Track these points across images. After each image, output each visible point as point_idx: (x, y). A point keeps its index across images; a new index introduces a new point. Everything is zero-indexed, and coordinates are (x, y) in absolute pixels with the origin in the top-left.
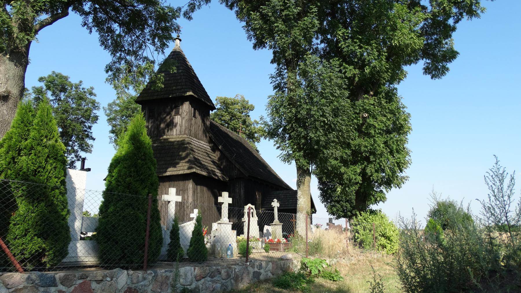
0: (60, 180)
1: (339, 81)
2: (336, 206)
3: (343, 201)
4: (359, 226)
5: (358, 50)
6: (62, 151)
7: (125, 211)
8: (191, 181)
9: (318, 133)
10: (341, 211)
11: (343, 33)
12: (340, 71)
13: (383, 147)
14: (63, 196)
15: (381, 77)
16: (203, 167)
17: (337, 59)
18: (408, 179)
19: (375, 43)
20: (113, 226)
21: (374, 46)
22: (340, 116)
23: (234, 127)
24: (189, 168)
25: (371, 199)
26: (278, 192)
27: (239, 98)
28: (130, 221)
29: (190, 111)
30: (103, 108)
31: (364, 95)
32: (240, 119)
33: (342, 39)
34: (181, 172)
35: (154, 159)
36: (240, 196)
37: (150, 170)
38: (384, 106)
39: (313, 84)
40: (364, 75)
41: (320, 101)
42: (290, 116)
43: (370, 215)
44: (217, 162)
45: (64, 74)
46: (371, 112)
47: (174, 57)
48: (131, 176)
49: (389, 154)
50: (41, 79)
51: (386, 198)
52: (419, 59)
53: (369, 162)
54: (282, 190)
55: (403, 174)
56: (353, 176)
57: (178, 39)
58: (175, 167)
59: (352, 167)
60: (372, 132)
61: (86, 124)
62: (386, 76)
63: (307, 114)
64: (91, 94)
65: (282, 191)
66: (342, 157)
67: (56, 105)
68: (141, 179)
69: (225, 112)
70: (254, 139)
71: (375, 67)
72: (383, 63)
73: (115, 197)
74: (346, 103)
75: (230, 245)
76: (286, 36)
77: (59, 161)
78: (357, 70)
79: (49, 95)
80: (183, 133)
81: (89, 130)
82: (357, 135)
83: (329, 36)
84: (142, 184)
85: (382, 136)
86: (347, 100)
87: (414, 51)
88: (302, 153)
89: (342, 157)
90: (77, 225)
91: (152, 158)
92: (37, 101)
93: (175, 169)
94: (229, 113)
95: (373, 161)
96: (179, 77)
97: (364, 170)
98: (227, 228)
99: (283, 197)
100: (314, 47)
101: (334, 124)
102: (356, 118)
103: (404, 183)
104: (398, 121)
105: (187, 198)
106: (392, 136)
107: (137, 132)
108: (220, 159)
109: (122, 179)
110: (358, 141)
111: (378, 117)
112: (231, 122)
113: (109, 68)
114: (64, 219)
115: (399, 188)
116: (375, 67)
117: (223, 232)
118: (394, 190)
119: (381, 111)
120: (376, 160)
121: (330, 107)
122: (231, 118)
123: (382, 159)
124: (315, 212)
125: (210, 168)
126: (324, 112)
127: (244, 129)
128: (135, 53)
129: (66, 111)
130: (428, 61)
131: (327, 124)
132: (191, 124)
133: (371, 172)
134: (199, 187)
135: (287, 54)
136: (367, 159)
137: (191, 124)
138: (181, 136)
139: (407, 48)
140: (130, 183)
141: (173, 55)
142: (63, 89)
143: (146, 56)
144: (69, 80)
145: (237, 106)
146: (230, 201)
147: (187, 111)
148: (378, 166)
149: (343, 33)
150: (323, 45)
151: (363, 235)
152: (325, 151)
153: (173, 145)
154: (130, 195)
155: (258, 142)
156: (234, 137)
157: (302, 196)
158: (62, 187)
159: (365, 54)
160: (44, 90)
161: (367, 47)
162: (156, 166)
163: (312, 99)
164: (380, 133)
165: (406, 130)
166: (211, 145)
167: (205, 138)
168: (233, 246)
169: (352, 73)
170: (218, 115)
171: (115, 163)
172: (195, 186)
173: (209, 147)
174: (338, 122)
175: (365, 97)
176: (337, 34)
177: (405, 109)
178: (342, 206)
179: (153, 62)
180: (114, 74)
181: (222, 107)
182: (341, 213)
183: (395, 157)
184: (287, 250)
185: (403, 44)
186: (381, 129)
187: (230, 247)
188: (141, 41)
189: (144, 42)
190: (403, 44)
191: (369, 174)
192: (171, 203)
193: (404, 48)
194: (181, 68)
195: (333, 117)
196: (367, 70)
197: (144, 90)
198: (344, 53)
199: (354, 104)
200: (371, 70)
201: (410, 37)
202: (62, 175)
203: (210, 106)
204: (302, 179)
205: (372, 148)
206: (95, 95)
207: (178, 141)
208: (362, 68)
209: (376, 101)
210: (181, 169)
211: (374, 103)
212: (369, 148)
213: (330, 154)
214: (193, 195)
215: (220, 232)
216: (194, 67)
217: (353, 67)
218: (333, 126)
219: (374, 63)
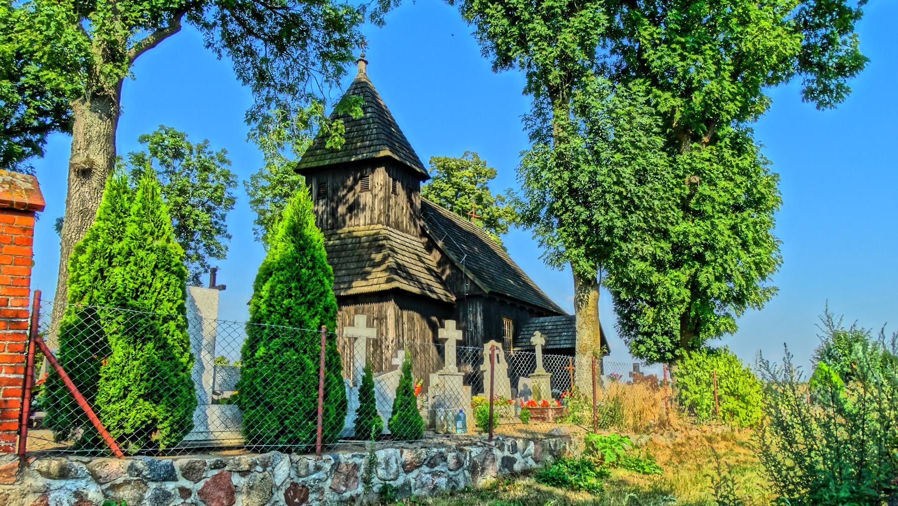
0: (176, 306)
1: (646, 120)
3: (657, 334)
6: (178, 257)
8: (392, 302)
10: (655, 352)
14: (181, 332)
16: (410, 277)
24: (389, 280)
26: (542, 319)
29: (386, 184)
32: (473, 193)
33: (649, 46)
36: (475, 327)
37: (323, 284)
44: (435, 269)
48: (290, 296)
49: (740, 247)
53: (704, 263)
54: (547, 316)
55: (767, 284)
59: (674, 273)
60: (708, 208)
61: (216, 212)
63: (590, 181)
73: (266, 331)
74: (659, 160)
78: (678, 99)
81: (221, 222)
85: (727, 216)
86: (661, 153)
87: (784, 59)
89: (654, 256)
93: (364, 283)
94: (453, 184)
95: (712, 261)
96: (366, 126)
97: (694, 277)
98: (455, 382)
101: (638, 197)
102: (678, 185)
105: (387, 333)
110: (683, 226)
113: (252, 117)
115: (759, 309)
117: (449, 389)
118: (750, 311)
122: (457, 193)
125: (423, 281)
126: (619, 176)
128: (291, 89)
131: (626, 198)
132: (389, 206)
134: (405, 313)
136: (699, 257)
138: (372, 226)
140: (290, 308)
142: (178, 154)
148: (720, 269)
149: (651, 35)
153: (360, 242)
154: (290, 328)
158: (180, 317)
159: (693, 70)
161: (694, 57)
162: (333, 278)
164: (723, 211)
174: (645, 192)
178: (656, 343)
182: (655, 355)
186: (724, 204)
187: (461, 414)
199: (674, 161)
200: (704, 97)
201: (775, 33)
208: (687, 94)
217: (670, 94)
219: (711, 85)
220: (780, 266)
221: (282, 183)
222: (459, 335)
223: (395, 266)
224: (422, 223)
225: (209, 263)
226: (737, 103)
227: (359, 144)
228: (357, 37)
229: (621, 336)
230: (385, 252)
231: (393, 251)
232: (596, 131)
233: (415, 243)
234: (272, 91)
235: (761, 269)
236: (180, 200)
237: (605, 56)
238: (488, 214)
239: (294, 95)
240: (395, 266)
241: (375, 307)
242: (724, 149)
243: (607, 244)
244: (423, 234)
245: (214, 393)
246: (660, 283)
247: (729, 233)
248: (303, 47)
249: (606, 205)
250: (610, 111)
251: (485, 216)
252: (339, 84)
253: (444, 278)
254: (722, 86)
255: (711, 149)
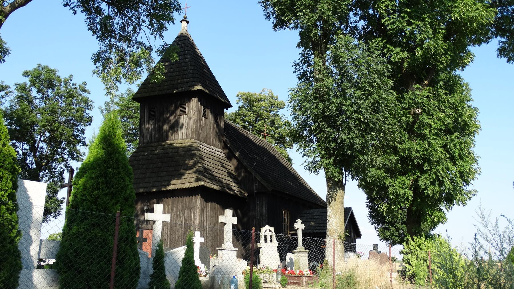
0: (7, 194)
1: (380, 68)
2: (390, 229)
3: (398, 223)
4: (410, 255)
5: (407, 27)
6: (11, 158)
7: (90, 232)
8: (199, 196)
9: (352, 134)
10: (397, 236)
11: (387, 6)
12: (383, 55)
13: (441, 152)
14: (11, 214)
15: (438, 62)
16: (213, 178)
17: (380, 39)
18: (476, 193)
19: (429, 17)
20: (75, 251)
21: (428, 21)
22: (381, 112)
23: (260, 129)
24: (197, 180)
25: (427, 220)
26: (311, 211)
27: (266, 94)
28: (96, 246)
29: (199, 110)
30: (100, 108)
31: (415, 84)
32: (268, 119)
33: (385, 14)
34: (187, 186)
35: (130, 167)
36: (262, 215)
37: (124, 181)
38: (442, 99)
39: (345, 71)
40: (415, 60)
41: (355, 93)
42: (316, 113)
43: (425, 241)
44: (233, 173)
45: (52, 67)
46: (425, 106)
47: (179, 43)
48: (99, 189)
49: (448, 160)
50: (25, 74)
51: (446, 218)
52: (491, 38)
53: (423, 172)
54: (316, 208)
55: (470, 188)
56: (401, 189)
57: (185, 21)
58: (180, 178)
59: (401, 179)
60: (427, 132)
61: (79, 127)
62: (444, 59)
63: (338, 110)
64: (84, 91)
65: (317, 210)
66: (384, 165)
67: (42, 105)
68: (112, 192)
69: (249, 111)
70: (285, 145)
71: (429, 48)
72: (440, 42)
73: (79, 214)
74: (391, 96)
75: (234, 277)
76: (312, 11)
77: (7, 170)
78: (406, 53)
79: (34, 92)
80: (190, 137)
81: (81, 135)
82: (407, 136)
83: (371, 11)
84: (113, 199)
85: (440, 137)
86: (391, 91)
87: (482, 26)
88: (331, 161)
89: (384, 165)
90: (34, 250)
91: (127, 167)
92: (19, 100)
93: (179, 181)
94: (254, 112)
95: (428, 170)
96: (185, 68)
97: (417, 181)
98: (230, 255)
99: (317, 217)
100: (352, 25)
101: (372, 122)
102: (404, 115)
103: (470, 199)
104: (461, 118)
105: (195, 219)
106: (453, 137)
107: (109, 133)
108: (237, 169)
109: (88, 192)
110: (407, 144)
111: (434, 113)
112: (255, 123)
113: (97, 58)
114: (12, 241)
115: (464, 206)
116: (429, 48)
117: (225, 261)
118: (457, 208)
119: (439, 106)
120: (431, 169)
121: (367, 101)
122: (256, 118)
123: (440, 168)
124: (359, 235)
125: (224, 181)
126: (359, 106)
127: (273, 132)
128: (127, 39)
129: (53, 112)
130: (503, 40)
131: (364, 123)
132: (200, 126)
133: (425, 185)
134: (209, 204)
135: (312, 35)
136: (420, 167)
137: (200, 126)
138: (187, 141)
139: (471, 22)
140: (98, 198)
141: (179, 41)
142: (51, 85)
143: (141, 41)
144: (58, 74)
145: (263, 104)
146: (235, 220)
147: (195, 109)
148: (434, 176)
149: (387, 6)
150: (362, 23)
151: (416, 267)
152: (361, 158)
153: (178, 152)
154: (98, 213)
155: (290, 148)
156: (256, 142)
157: (333, 216)
158: (10, 203)
159: (416, 32)
160: (28, 86)
161: (418, 23)
162: (133, 176)
163: (343, 90)
164: (437, 134)
165: (472, 129)
166: (225, 151)
167: (218, 143)
168: (238, 279)
169: (399, 57)
170: (240, 115)
171: (81, 172)
172: (205, 202)
173: (223, 155)
174: (378, 119)
175: (415, 87)
176: (379, 7)
177: (470, 103)
178: (397, 230)
179: (149, 48)
180: (103, 65)
181: (245, 105)
182: (397, 238)
183: (457, 165)
184: (311, 285)
185: (466, 17)
186: (438, 129)
187: (234, 280)
188: (135, 23)
189: (138, 25)
190: (466, 17)
191: (423, 187)
192: (157, 224)
193: (467, 23)
194: (188, 56)
195: (371, 114)
196: (418, 52)
197: (143, 84)
198: (388, 31)
199: (402, 97)
200: (424, 52)
201: (475, 8)
202: (10, 187)
203: (225, 103)
204: (333, 194)
205: (426, 153)
206: (89, 93)
207: (184, 147)
208: (412, 51)
209: (431, 93)
210: (187, 182)
211: (428, 95)
212: (421, 153)
213: (369, 161)
214: (201, 214)
215: (221, 261)
216: (204, 56)
217: (400, 49)
218: (371, 125)
219: (428, 43)
220: (479, 175)
221: (128, 108)
222: (303, 226)
223: (202, 169)
224: (225, 139)
225: (71, 165)
226: (448, 56)
227: (180, 81)
228: (175, 4)
229: (372, 224)
230: (196, 159)
231: (202, 159)
232: (343, 74)
233: (218, 153)
234: (113, 40)
235: (464, 176)
236: (51, 118)
237: (356, 22)
238: (279, 134)
239: (129, 43)
240: (202, 169)
241: (187, 199)
242: (440, 90)
243: (350, 156)
244: (225, 147)
245: (40, 260)
246: (390, 185)
247: (442, 150)
248: (137, 9)
249: (349, 128)
250: (354, 60)
251: (276, 135)
252: (162, 36)
253: (240, 179)
254: (437, 44)
255: (430, 89)
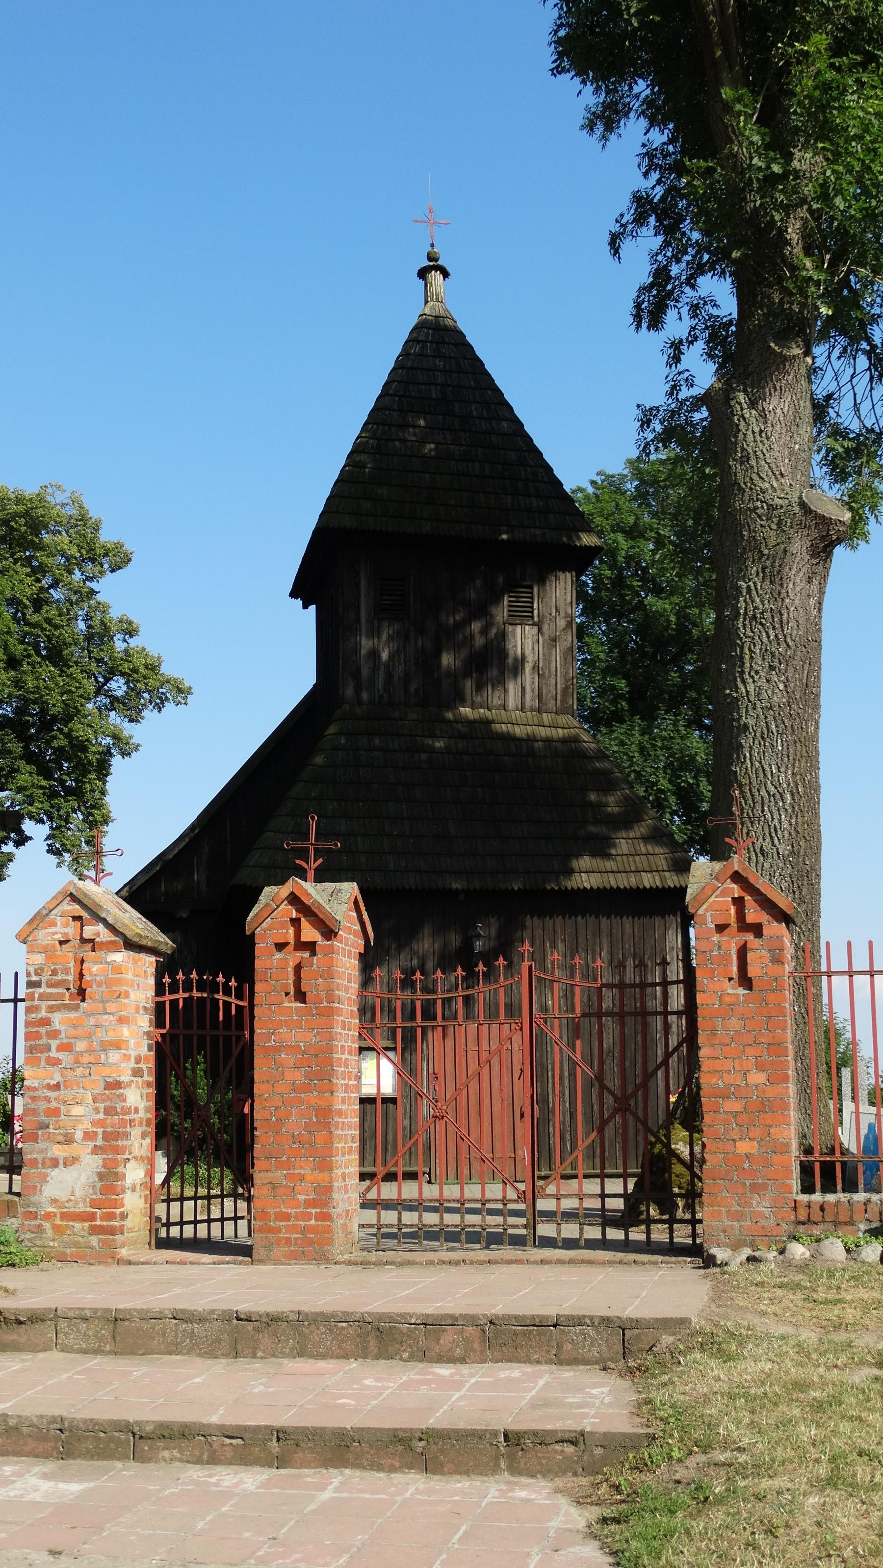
207: (548, 741)
